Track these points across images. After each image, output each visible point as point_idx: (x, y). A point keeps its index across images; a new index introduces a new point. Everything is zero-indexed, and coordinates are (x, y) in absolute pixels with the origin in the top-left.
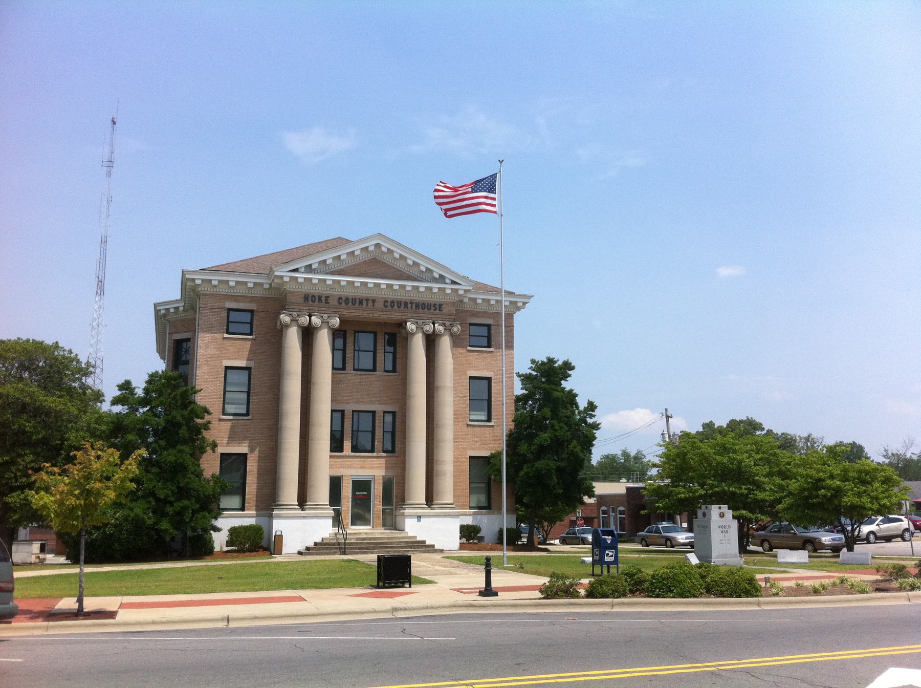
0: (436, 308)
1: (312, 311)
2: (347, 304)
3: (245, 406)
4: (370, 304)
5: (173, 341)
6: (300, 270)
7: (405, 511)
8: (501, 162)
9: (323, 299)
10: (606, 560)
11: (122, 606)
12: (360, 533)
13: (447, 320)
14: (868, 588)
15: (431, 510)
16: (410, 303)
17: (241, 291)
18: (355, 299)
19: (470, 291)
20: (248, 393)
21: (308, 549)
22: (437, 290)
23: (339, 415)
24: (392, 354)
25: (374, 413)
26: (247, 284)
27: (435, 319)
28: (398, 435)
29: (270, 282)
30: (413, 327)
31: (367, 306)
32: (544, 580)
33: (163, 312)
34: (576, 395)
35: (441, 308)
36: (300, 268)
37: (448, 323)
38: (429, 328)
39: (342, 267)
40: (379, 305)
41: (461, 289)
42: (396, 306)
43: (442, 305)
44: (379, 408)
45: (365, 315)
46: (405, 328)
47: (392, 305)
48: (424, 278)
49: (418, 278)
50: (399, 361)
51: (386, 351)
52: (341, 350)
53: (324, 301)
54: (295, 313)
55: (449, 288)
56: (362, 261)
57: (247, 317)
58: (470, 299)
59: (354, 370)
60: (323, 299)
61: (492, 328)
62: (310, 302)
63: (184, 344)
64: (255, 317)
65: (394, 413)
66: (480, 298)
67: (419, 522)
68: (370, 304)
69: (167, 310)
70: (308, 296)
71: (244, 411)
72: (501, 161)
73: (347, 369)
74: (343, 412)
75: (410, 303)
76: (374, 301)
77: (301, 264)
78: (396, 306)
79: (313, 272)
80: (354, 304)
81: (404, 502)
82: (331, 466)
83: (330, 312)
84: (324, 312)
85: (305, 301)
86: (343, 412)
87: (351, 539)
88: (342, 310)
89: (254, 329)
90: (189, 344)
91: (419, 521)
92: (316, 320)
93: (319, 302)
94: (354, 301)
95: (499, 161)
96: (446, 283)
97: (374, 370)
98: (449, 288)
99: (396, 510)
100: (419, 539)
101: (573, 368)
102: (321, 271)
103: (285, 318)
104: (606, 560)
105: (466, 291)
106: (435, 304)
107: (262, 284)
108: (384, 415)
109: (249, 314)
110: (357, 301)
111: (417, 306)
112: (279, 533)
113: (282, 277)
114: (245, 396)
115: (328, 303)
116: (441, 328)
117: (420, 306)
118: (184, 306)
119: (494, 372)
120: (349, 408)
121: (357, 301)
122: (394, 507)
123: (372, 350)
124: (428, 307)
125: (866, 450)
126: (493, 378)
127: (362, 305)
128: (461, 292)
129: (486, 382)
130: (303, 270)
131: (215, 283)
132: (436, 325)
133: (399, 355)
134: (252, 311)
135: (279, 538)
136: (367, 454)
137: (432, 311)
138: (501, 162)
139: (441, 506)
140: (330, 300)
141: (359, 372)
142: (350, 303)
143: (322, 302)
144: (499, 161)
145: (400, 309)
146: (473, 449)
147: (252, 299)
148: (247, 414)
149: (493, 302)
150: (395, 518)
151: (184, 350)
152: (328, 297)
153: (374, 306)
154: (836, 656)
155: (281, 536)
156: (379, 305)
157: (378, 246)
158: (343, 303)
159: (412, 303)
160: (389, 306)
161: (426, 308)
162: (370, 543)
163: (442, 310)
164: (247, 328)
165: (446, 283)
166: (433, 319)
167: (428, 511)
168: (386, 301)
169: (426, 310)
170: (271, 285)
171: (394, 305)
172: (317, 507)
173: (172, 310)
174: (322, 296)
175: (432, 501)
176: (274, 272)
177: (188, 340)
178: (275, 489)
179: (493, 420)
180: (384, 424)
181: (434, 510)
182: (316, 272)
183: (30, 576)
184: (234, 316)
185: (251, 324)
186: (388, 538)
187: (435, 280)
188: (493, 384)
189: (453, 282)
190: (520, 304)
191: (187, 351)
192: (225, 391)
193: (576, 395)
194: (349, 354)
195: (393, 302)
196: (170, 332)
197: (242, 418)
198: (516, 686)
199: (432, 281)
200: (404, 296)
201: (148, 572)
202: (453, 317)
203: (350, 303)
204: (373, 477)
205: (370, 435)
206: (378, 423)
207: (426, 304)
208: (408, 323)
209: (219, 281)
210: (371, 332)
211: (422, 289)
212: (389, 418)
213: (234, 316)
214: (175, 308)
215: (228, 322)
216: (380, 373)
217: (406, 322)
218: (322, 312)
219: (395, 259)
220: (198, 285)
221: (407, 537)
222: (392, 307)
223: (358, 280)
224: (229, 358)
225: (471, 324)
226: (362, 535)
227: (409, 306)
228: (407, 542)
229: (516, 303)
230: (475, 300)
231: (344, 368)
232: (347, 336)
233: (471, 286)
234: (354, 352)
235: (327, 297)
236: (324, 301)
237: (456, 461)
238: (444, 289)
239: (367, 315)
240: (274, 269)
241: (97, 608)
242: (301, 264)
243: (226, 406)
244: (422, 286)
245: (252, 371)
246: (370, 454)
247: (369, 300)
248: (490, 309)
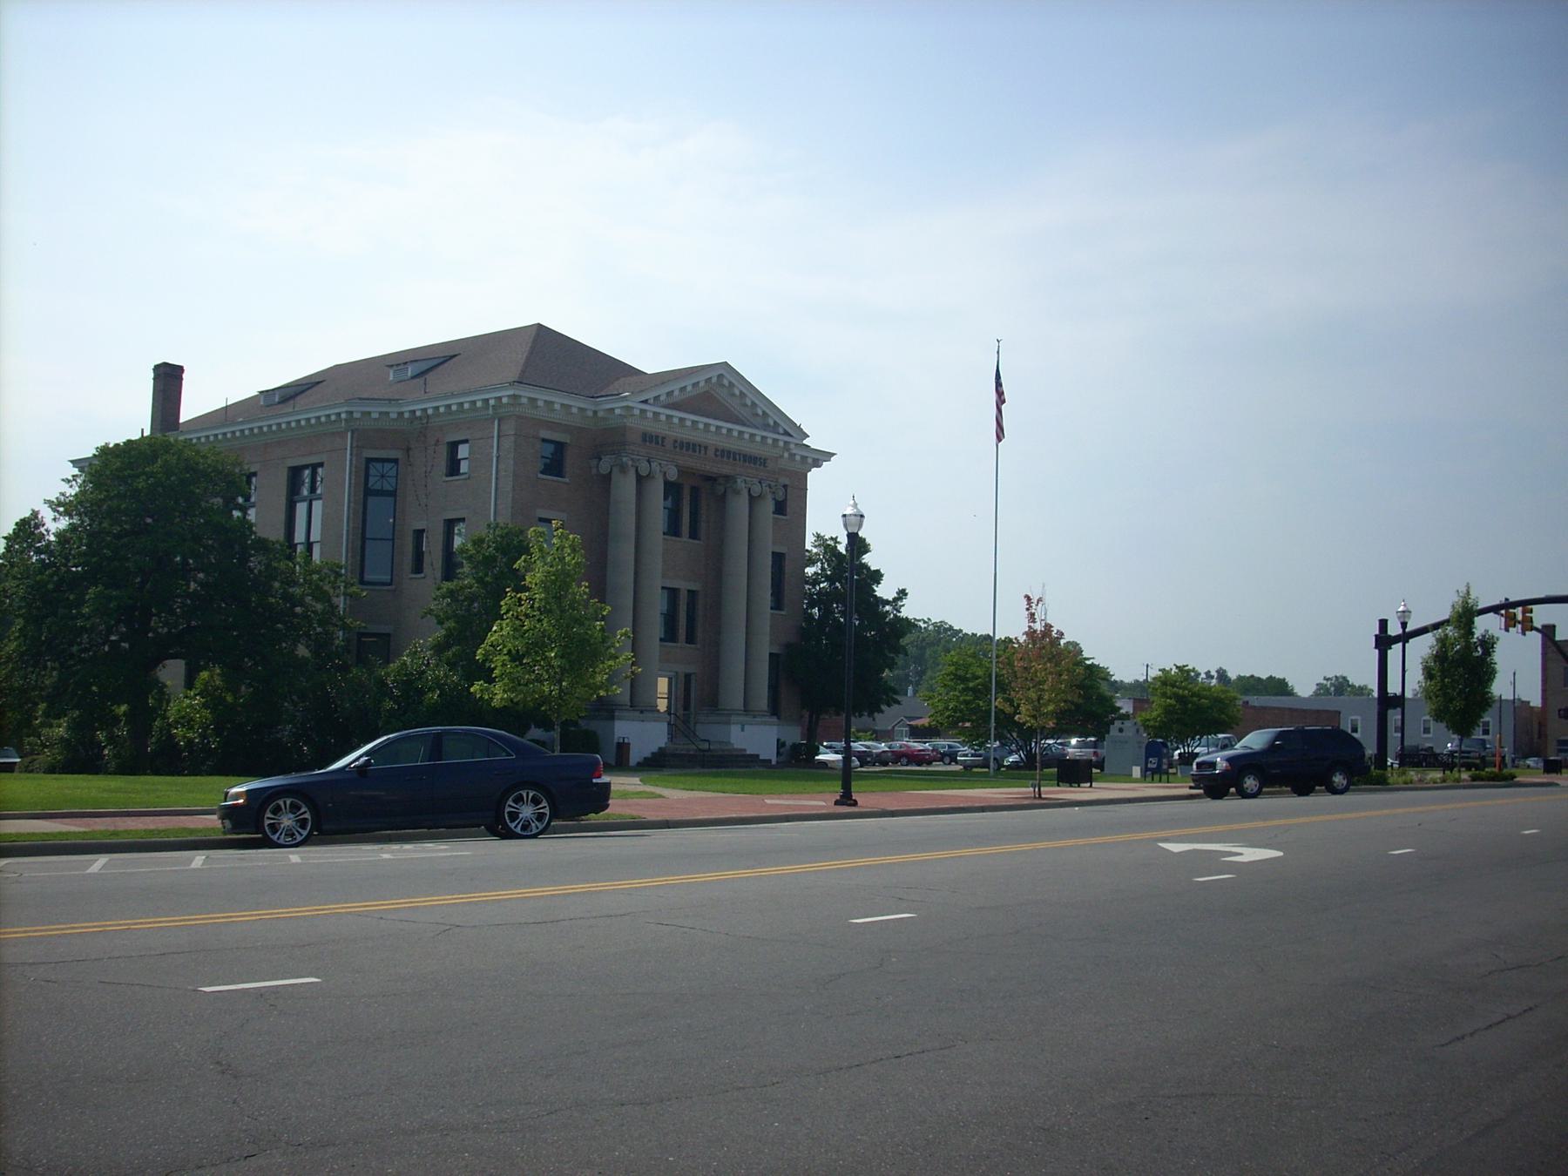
2: (681, 448)
6: (649, 402)
10: (1134, 768)
14: (1438, 780)
22: (652, 414)
32: (1515, 780)
40: (711, 453)
53: (660, 442)
76: (706, 448)
104: (1134, 768)
125: (1204, 663)
142: (684, 449)
149: (574, 410)
154: (611, 885)
156: (711, 453)
157: (720, 376)
183: (72, 830)
187: (766, 427)
189: (787, 433)
197: (386, 588)
198: (1400, 854)
203: (684, 449)
216: (685, 539)
222: (722, 457)
235: (663, 438)
242: (650, 395)
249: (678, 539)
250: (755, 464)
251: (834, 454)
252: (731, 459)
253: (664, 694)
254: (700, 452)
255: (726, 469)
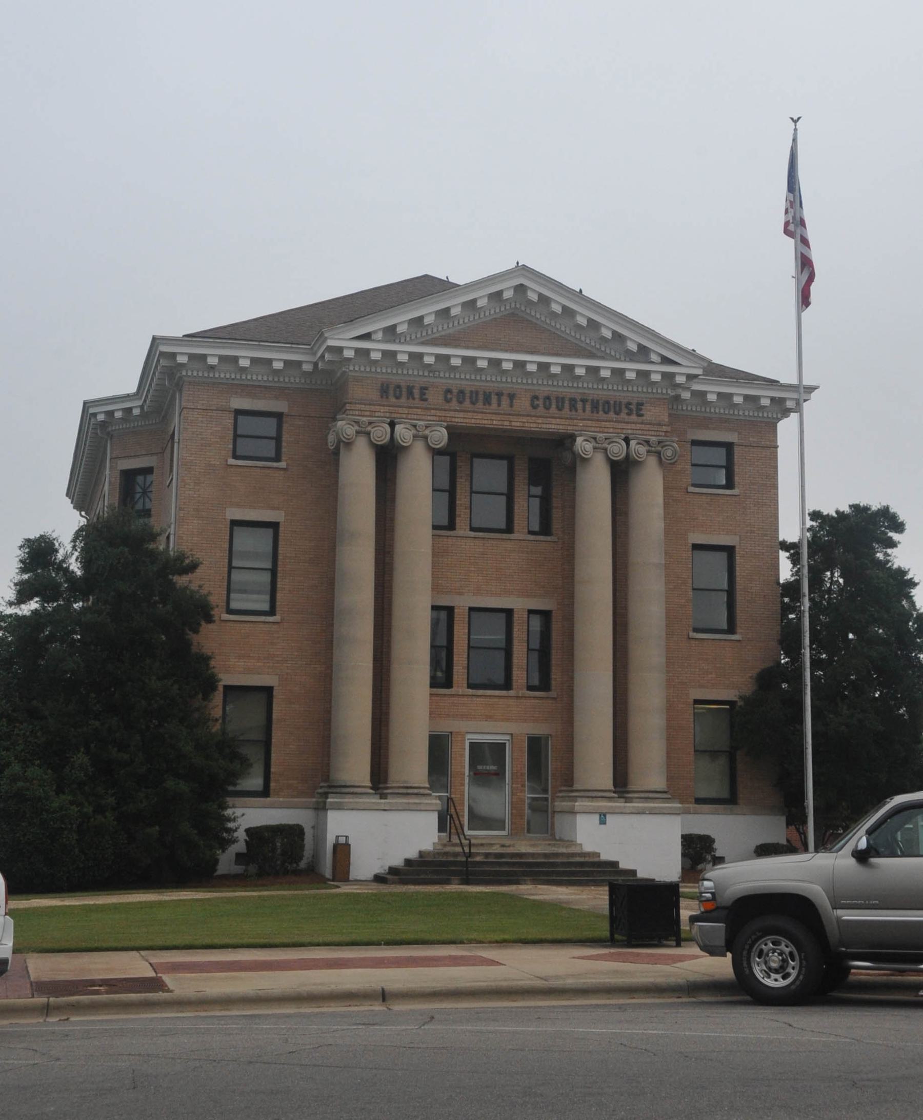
0: (631, 410)
1: (399, 416)
3: (267, 597)
4: (505, 401)
5: (118, 475)
6: (374, 337)
7: (577, 804)
8: (795, 121)
9: (416, 393)
11: (176, 968)
12: (492, 845)
13: (653, 433)
15: (626, 802)
16: (497, 394)
17: (259, 376)
18: (477, 393)
19: (696, 376)
20: (274, 572)
21: (393, 871)
23: (443, 615)
24: (447, 493)
25: (509, 613)
26: (272, 364)
27: (630, 432)
28: (556, 657)
29: (315, 360)
30: (589, 446)
31: (499, 405)
33: (101, 417)
34: (912, 584)
35: (641, 410)
36: (375, 332)
37: (654, 438)
38: (618, 450)
39: (451, 331)
41: (681, 375)
42: (554, 406)
43: (642, 404)
44: (519, 604)
45: (495, 422)
46: (571, 449)
47: (547, 403)
48: (608, 351)
49: (594, 351)
50: (556, 514)
51: (474, 489)
52: (502, 494)
53: (417, 396)
54: (365, 419)
55: (656, 371)
56: (488, 319)
57: (268, 427)
58: (695, 393)
59: (472, 529)
60: (416, 393)
61: (737, 450)
62: (393, 400)
63: (140, 479)
64: (285, 426)
65: (546, 615)
66: (712, 390)
67: (603, 826)
68: (505, 401)
69: (110, 414)
70: (388, 387)
71: (266, 607)
72: (795, 118)
73: (457, 527)
74: (450, 610)
75: (497, 394)
76: (512, 397)
77: (376, 325)
78: (554, 406)
79: (397, 341)
80: (560, 409)
81: (572, 786)
82: (433, 715)
83: (429, 418)
84: (418, 417)
85: (382, 397)
86: (450, 610)
87: (478, 854)
88: (452, 414)
89: (284, 450)
90: (149, 478)
91: (603, 822)
92: (403, 433)
93: (408, 398)
94: (474, 395)
95: (792, 119)
96: (652, 362)
97: (509, 529)
98: (656, 371)
99: (553, 800)
100: (604, 857)
101: (899, 527)
102: (413, 337)
103: (344, 427)
105: (690, 377)
106: (629, 404)
107: (299, 364)
108: (528, 618)
109: (273, 422)
110: (481, 397)
111: (595, 406)
112: (342, 840)
113: (340, 350)
114: (266, 578)
115: (426, 400)
116: (643, 450)
117: (601, 408)
118: (142, 407)
119: (740, 536)
120: (463, 603)
121: (481, 397)
122: (549, 796)
123: (505, 490)
124: (615, 407)
126: (737, 547)
127: (490, 404)
128: (680, 380)
129: (723, 556)
130: (380, 336)
131: (278, 365)
132: (633, 443)
133: (556, 502)
134: (279, 416)
135: (342, 850)
136: (497, 693)
137: (623, 415)
138: (795, 121)
139: (646, 795)
140: (429, 395)
141: (481, 534)
143: (414, 399)
144: (792, 119)
145: (563, 412)
146: (701, 686)
147: (281, 392)
148: (272, 612)
149: (712, 398)
150: (553, 817)
151: (139, 489)
152: (426, 388)
153: (511, 406)
155: (347, 846)
157: (521, 289)
158: (454, 399)
159: (584, 401)
160: (541, 405)
161: (612, 410)
162: (514, 864)
163: (642, 415)
164: (269, 448)
165: (652, 362)
166: (624, 431)
167: (620, 804)
168: (536, 397)
169: (612, 415)
170: (316, 365)
171: (550, 405)
172: (408, 791)
173: (118, 415)
174: (413, 387)
175: (386, 781)
176: (326, 338)
177: (149, 471)
178: (328, 755)
179: (739, 630)
180: (528, 635)
181: (631, 802)
182: (402, 341)
184: (247, 425)
185: (278, 439)
186: (545, 855)
187: (630, 356)
188: (738, 559)
189: (666, 360)
190: (790, 404)
191: (145, 492)
192: (230, 567)
193: (912, 584)
194: (462, 499)
195: (548, 398)
196: (114, 456)
197: (262, 618)
199: (623, 358)
200: (441, 378)
201: (116, 907)
202: (664, 429)
203: (468, 401)
204: (508, 737)
205: (500, 656)
206: (519, 633)
207: (612, 402)
208: (579, 440)
209: (254, 361)
210: (500, 457)
211: (605, 374)
212: (536, 623)
213: (247, 425)
214: (124, 410)
215: (236, 436)
216: (521, 537)
217: (572, 438)
218: (415, 417)
219: (554, 314)
220: (182, 365)
221: (573, 855)
222: (547, 408)
223: (483, 357)
224: (238, 505)
225: (695, 443)
226: (495, 848)
227: (579, 405)
228: (582, 864)
229: (782, 401)
230: (703, 394)
231: (451, 526)
232: (459, 464)
233: (700, 368)
234: (471, 496)
235: (423, 390)
236: (417, 396)
237: (670, 709)
238: (646, 374)
239: (500, 423)
240: (326, 335)
241: (651, 980)
243: (232, 595)
244: (606, 367)
245: (281, 529)
246: (504, 693)
247: (502, 394)
248: (708, 410)
249: (549, 538)
250: (617, 413)
251: (816, 388)
252: (601, 413)
253: (609, 791)
254: (584, 411)
255: (555, 425)
